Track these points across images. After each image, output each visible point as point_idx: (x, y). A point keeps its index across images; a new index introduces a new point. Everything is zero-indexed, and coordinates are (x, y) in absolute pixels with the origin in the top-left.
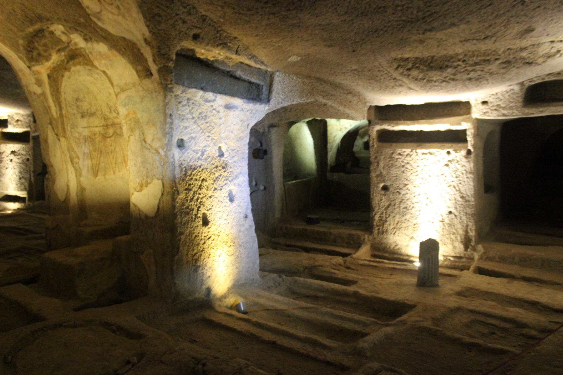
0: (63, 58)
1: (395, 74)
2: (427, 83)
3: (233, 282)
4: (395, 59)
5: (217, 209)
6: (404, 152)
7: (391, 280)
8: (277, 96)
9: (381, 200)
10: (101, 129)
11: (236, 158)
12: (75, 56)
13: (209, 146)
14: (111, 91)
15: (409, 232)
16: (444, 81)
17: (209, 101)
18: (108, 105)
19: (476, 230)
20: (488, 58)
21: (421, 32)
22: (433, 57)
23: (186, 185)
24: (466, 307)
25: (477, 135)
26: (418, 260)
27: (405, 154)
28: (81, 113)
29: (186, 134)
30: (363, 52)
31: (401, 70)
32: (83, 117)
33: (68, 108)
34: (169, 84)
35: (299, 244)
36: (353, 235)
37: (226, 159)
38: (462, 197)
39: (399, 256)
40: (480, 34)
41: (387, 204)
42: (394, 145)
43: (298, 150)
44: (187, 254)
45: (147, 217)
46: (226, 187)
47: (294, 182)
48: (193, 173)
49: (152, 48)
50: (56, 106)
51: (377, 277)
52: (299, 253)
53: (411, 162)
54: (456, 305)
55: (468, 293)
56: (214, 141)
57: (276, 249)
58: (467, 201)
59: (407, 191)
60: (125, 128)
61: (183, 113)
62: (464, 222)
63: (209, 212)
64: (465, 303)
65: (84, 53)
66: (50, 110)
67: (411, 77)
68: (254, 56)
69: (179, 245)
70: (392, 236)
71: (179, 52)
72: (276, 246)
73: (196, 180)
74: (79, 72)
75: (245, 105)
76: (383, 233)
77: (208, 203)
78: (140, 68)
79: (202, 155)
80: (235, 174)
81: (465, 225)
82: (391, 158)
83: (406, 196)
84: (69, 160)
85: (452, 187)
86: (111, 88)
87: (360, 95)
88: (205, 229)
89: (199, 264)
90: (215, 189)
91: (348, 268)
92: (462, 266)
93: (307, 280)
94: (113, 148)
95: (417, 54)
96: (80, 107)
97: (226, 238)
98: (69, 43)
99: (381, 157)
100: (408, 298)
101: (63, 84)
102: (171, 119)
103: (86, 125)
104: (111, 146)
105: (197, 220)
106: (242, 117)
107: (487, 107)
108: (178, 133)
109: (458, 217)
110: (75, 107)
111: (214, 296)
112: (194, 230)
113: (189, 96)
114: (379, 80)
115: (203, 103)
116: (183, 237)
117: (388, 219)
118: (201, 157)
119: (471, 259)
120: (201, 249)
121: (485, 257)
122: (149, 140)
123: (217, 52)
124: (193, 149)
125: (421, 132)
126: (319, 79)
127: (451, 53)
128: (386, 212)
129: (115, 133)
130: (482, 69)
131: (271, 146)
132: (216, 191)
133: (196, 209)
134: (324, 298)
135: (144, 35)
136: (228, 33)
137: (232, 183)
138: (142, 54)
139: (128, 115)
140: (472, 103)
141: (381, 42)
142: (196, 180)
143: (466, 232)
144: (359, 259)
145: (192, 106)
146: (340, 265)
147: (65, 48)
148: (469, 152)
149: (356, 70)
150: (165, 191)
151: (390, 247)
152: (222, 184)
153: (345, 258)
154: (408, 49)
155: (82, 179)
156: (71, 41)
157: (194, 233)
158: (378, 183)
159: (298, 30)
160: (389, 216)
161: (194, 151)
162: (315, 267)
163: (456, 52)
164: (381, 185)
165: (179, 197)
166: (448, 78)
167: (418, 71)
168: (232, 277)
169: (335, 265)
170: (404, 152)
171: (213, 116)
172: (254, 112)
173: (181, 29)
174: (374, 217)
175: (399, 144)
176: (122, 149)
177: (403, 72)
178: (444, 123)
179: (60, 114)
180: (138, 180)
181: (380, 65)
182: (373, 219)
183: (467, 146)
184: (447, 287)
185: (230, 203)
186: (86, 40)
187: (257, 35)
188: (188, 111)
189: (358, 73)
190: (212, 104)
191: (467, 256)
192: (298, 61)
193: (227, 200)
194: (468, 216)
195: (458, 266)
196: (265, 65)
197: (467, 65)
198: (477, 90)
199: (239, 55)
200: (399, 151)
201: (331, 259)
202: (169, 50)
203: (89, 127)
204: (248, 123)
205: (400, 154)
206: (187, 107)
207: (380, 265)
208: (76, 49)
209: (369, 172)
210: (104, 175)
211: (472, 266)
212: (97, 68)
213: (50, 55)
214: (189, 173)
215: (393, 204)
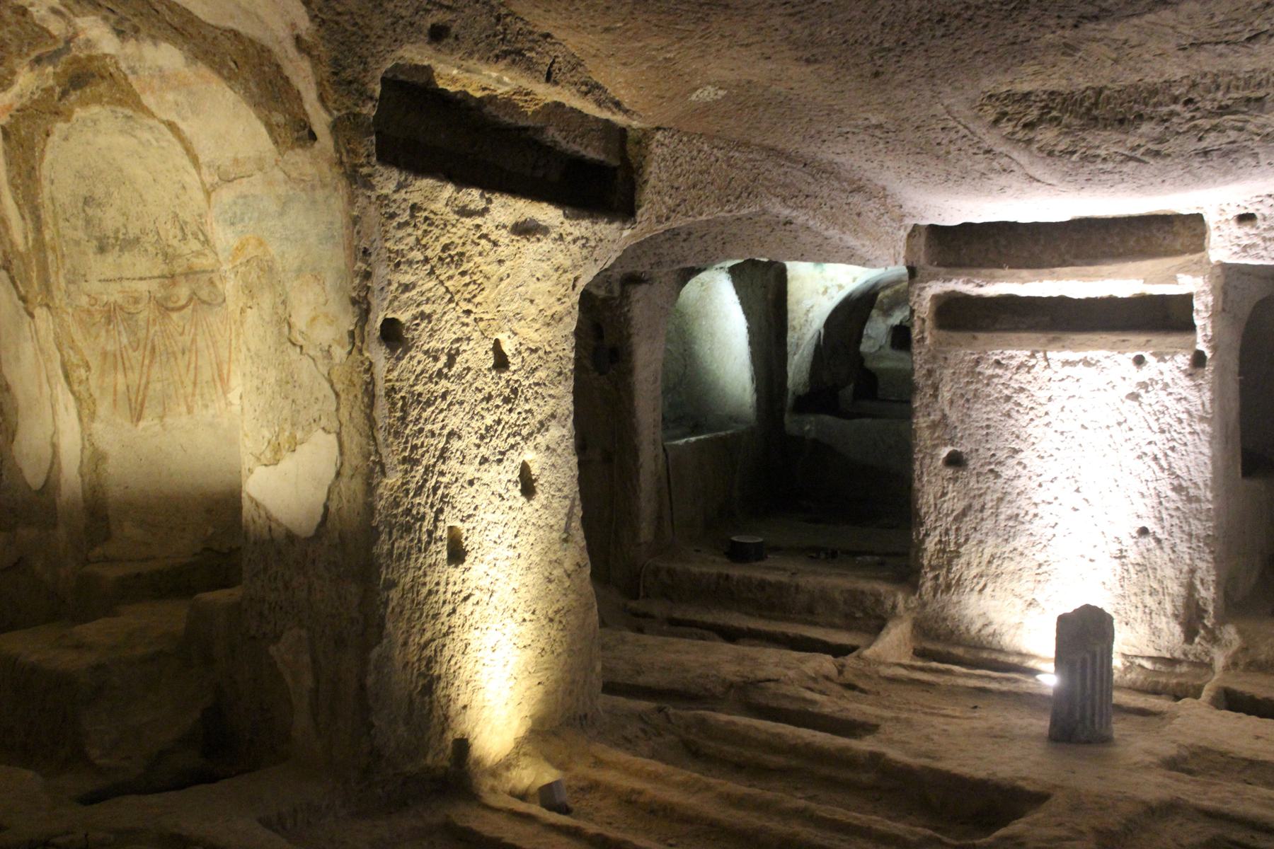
0: (51, 82)
1: (991, 139)
2: (1081, 164)
3: (529, 723)
4: (990, 96)
5: (489, 517)
6: (1012, 357)
7: (976, 724)
8: (656, 198)
9: (944, 494)
10: (154, 285)
11: (541, 374)
12: (83, 77)
13: (469, 339)
14: (191, 178)
15: (1024, 587)
16: (1131, 159)
17: (470, 214)
18: (176, 216)
19: (1218, 584)
20: (1261, 93)
21: (1070, 22)
22: (1099, 92)
23: (405, 449)
24: (1192, 801)
25: (1221, 311)
26: (1051, 667)
27: (1015, 363)
28: (97, 239)
29: (407, 305)
30: (902, 76)
31: (1007, 127)
32: (102, 249)
33: (62, 224)
34: (362, 166)
35: (708, 618)
36: (863, 592)
37: (515, 377)
38: (1178, 489)
39: (994, 656)
40: (1239, 28)
41: (960, 506)
42: (982, 336)
43: (704, 348)
44: (405, 644)
45: (291, 537)
46: (512, 454)
47: (693, 439)
48: (425, 415)
49: (316, 61)
50: (23, 218)
51: (932, 714)
52: (709, 643)
53: (1032, 388)
54: (1165, 794)
55: (1198, 761)
56: (482, 325)
57: (640, 630)
58: (1190, 499)
59: (1019, 468)
60: (230, 287)
61: (401, 247)
62: (1184, 562)
63: (467, 525)
64: (1187, 790)
65: (112, 70)
66: (7, 229)
67: (1035, 147)
68: (598, 87)
69: (383, 618)
70: (975, 595)
71: (390, 75)
72: (639, 622)
73: (433, 434)
74: (95, 122)
75: (567, 222)
76: (948, 587)
77: (463, 499)
78: (278, 118)
79: (451, 363)
80: (539, 417)
81: (1186, 569)
82: (973, 373)
83: (1015, 483)
84: (60, 372)
85: (1148, 460)
86: (193, 171)
87: (886, 197)
88: (455, 573)
89: (436, 671)
90: (484, 460)
91: (851, 687)
92: (1179, 684)
93: (736, 718)
94: (187, 339)
95: (1056, 83)
96: (96, 222)
97: (511, 600)
98: (68, 41)
99: (944, 367)
100: (1024, 774)
101: (48, 157)
102: (365, 262)
103: (109, 274)
104: (182, 334)
105: (433, 547)
106: (560, 258)
107: (1254, 231)
108: (386, 303)
109: (1166, 545)
110: (81, 223)
111: (478, 762)
112: (425, 575)
113: (416, 198)
114: (939, 155)
115: (453, 218)
116: (395, 594)
117: (962, 550)
118: (445, 370)
119: (1205, 666)
120: (445, 629)
121: (1246, 662)
122: (300, 322)
123: (494, 75)
124: (426, 347)
125: (1062, 301)
126: (772, 151)
127: (1152, 78)
128: (958, 529)
129: (193, 296)
130: (1240, 124)
131: (629, 336)
132: (486, 466)
133: (430, 515)
134: (784, 772)
135: (293, 26)
136: (527, 23)
137: (531, 444)
138: (287, 80)
139: (240, 249)
140: (1210, 219)
141: (955, 51)
142: (433, 434)
143: (1191, 588)
144: (880, 663)
145: (425, 227)
146: (827, 678)
147: (57, 54)
148: (1199, 360)
149: (879, 126)
150: (346, 464)
151: (968, 629)
152: (503, 446)
153: (841, 660)
154: (1030, 70)
155: (98, 427)
156: (76, 35)
157: (425, 584)
158: (935, 446)
159: (722, 17)
160: (967, 540)
161: (426, 352)
162: (756, 683)
163: (1166, 77)
164: (945, 452)
165: (386, 481)
166: (1142, 150)
167: (1056, 131)
168: (526, 710)
169: (815, 680)
170: (1012, 357)
171: (480, 254)
172: (593, 243)
173: (398, 11)
174: (922, 542)
175: (996, 336)
176: (214, 343)
177: (1013, 133)
178: (1126, 276)
179: (35, 240)
180: (267, 433)
181: (949, 113)
182: (919, 547)
183: (1195, 342)
184: (1135, 744)
185: (523, 499)
186: (120, 33)
187: (607, 30)
188: (411, 240)
189: (886, 136)
190: (478, 221)
191: (1191, 658)
192: (716, 101)
193: (516, 491)
194: (1194, 543)
195: (1166, 686)
196: (626, 112)
197: (1198, 114)
198: (1227, 183)
199: (556, 83)
200: (996, 355)
201: (801, 661)
202: (365, 70)
203: (121, 279)
204: (577, 273)
205: (998, 363)
206: (410, 230)
207: (942, 680)
208: (90, 59)
209: (909, 415)
210: (161, 418)
211: (1207, 687)
212: (152, 115)
213: (13, 73)
214: (414, 414)
215: (977, 506)
